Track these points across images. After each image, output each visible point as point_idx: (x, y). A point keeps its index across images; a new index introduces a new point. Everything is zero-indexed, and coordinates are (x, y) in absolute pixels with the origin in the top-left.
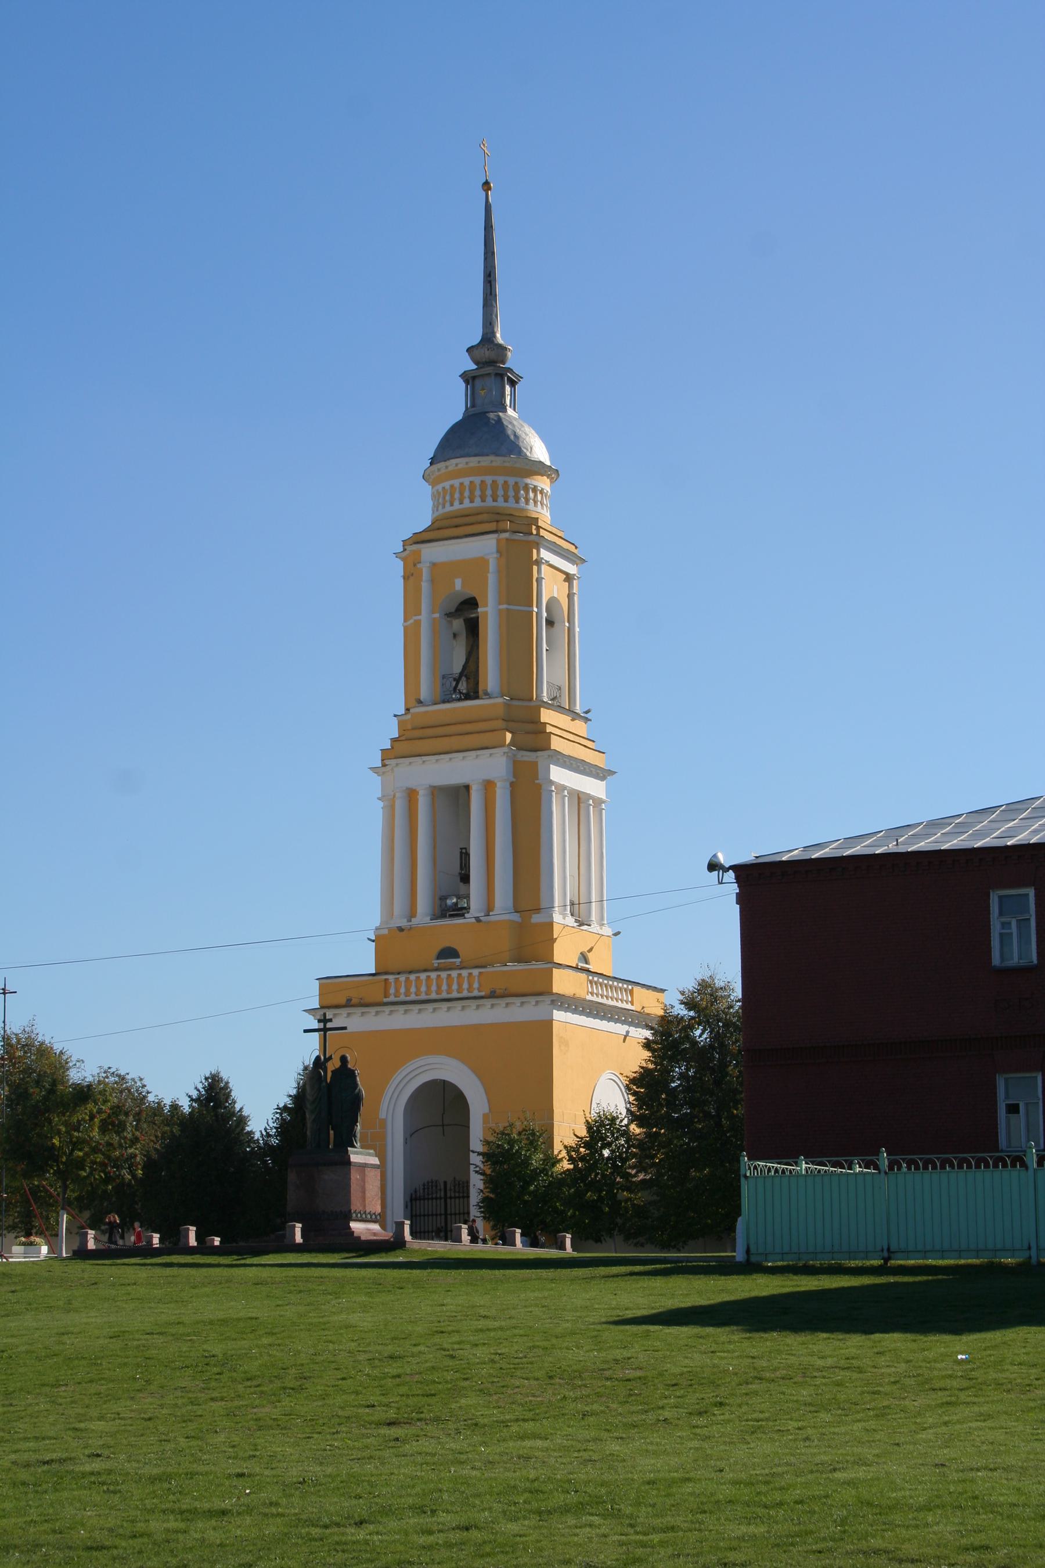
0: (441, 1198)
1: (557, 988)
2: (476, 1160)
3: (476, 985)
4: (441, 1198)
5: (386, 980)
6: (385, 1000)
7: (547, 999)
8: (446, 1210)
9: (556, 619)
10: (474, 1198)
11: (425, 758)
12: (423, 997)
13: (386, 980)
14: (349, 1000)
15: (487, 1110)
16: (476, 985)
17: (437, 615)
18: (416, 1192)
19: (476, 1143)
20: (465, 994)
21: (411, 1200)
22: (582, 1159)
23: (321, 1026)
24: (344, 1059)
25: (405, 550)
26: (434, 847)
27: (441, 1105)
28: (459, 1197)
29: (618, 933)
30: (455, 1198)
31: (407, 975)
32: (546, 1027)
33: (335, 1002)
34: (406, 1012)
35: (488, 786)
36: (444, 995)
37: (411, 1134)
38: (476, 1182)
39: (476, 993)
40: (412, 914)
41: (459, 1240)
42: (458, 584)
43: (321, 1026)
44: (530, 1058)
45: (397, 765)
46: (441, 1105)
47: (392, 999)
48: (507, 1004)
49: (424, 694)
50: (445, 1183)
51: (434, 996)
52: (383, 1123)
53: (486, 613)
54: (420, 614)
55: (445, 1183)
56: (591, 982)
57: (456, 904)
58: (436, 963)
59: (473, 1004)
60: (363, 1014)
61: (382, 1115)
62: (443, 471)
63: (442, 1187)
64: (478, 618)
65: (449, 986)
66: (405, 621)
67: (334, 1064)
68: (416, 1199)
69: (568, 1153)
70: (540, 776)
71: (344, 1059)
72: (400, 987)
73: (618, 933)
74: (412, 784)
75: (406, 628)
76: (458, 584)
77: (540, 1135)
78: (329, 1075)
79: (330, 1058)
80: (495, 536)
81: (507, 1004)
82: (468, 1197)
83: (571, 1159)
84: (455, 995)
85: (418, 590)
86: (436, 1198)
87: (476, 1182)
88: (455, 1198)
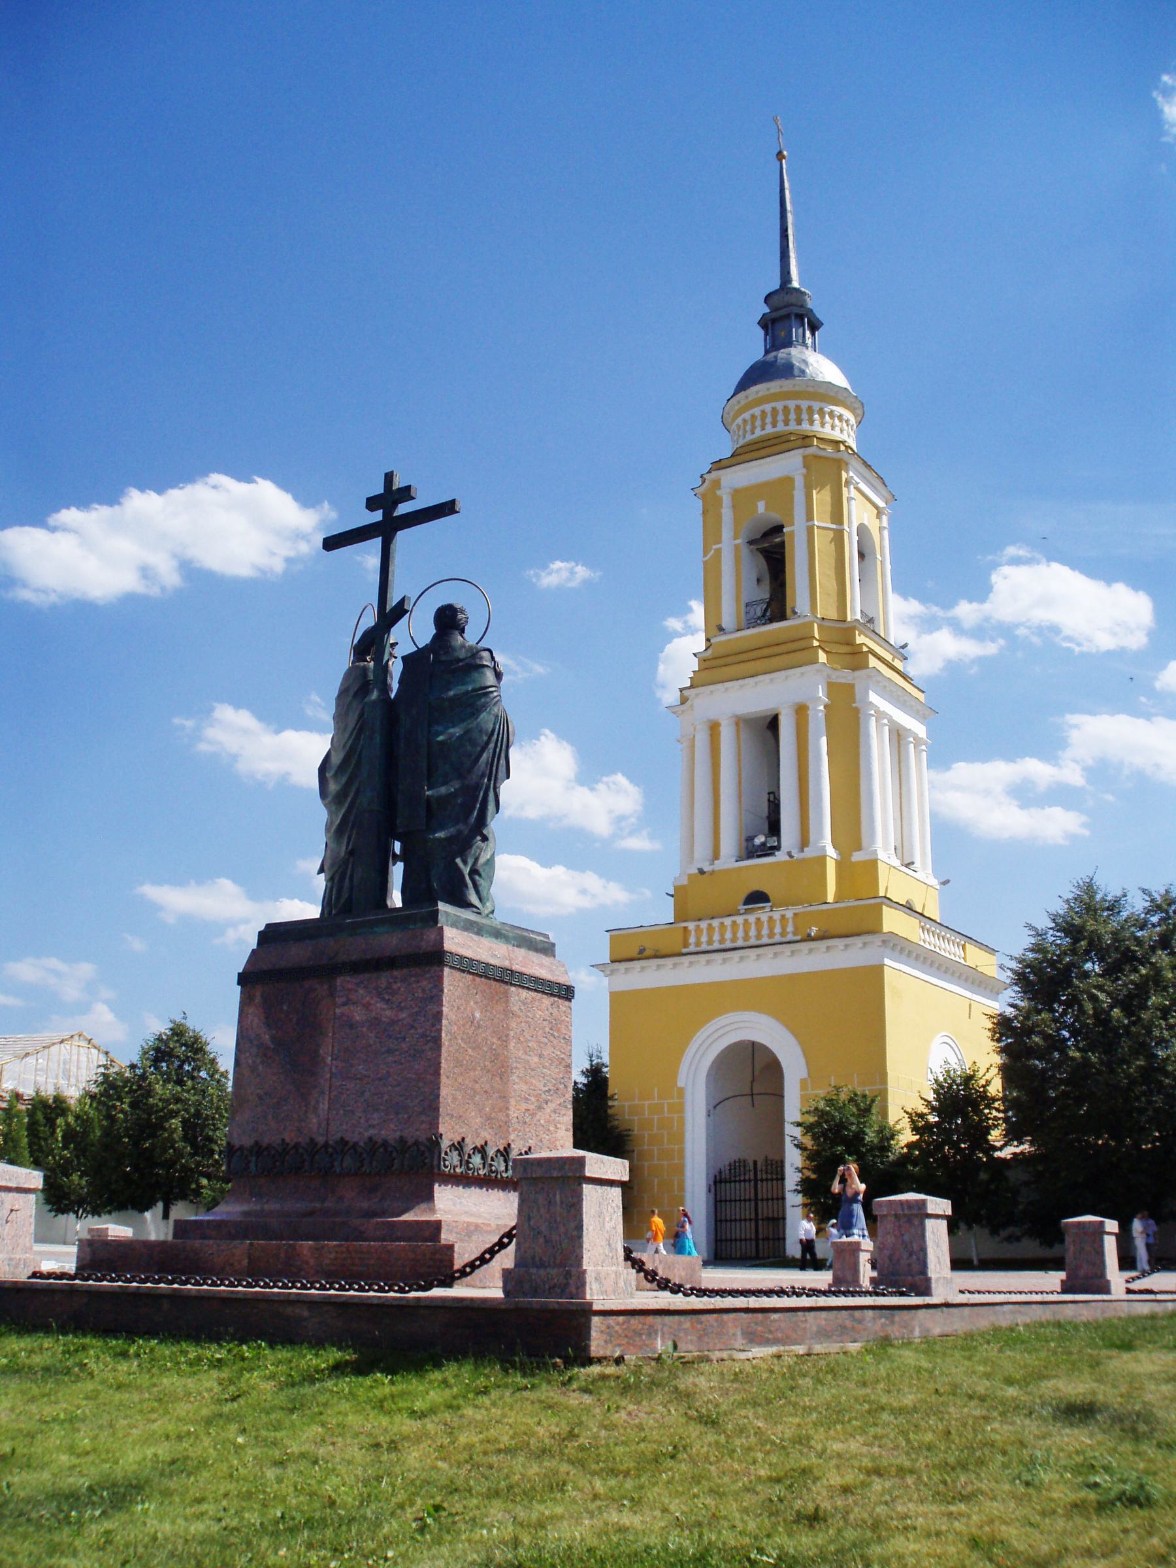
0: (750, 1181)
1: (886, 928)
2: (792, 1132)
3: (790, 929)
4: (750, 1181)
5: (685, 928)
6: (685, 951)
7: (877, 940)
8: (756, 1205)
9: (866, 552)
10: (792, 1179)
11: (727, 684)
12: (728, 945)
13: (685, 928)
14: (642, 951)
15: (804, 1075)
16: (790, 929)
17: (739, 541)
18: (720, 1172)
19: (793, 1110)
20: (777, 938)
21: (715, 1183)
22: (928, 1127)
23: (378, 516)
24: (448, 620)
25: (703, 482)
26: (739, 760)
27: (751, 1076)
28: (772, 1180)
29: (947, 882)
30: (767, 1180)
31: (709, 921)
32: (876, 974)
33: (629, 955)
34: (708, 962)
35: (801, 711)
36: (753, 942)
37: (715, 1106)
38: (794, 1159)
39: (790, 937)
40: (716, 856)
41: (1105, 1288)
42: (761, 507)
43: (378, 516)
44: (857, 1010)
45: (697, 695)
46: (751, 1076)
47: (692, 948)
48: (828, 948)
49: (728, 620)
50: (755, 1163)
51: (740, 943)
52: (681, 1092)
53: (792, 533)
54: (720, 542)
55: (755, 1163)
56: (923, 928)
57: (764, 844)
58: (742, 908)
59: (787, 949)
60: (659, 967)
61: (680, 1084)
62: (743, 403)
63: (752, 1167)
64: (783, 543)
65: (759, 931)
66: (705, 554)
67: (413, 634)
68: (721, 1182)
69: (913, 1121)
70: (858, 696)
71: (448, 620)
72: (700, 932)
73: (947, 882)
74: (713, 715)
75: (705, 563)
76: (761, 507)
77: (868, 1105)
78: (396, 668)
79: (400, 611)
80: (801, 451)
81: (828, 948)
82: (783, 1179)
83: (916, 1129)
84: (765, 940)
85: (719, 517)
86: (745, 1181)
87: (794, 1159)
88: (767, 1180)
